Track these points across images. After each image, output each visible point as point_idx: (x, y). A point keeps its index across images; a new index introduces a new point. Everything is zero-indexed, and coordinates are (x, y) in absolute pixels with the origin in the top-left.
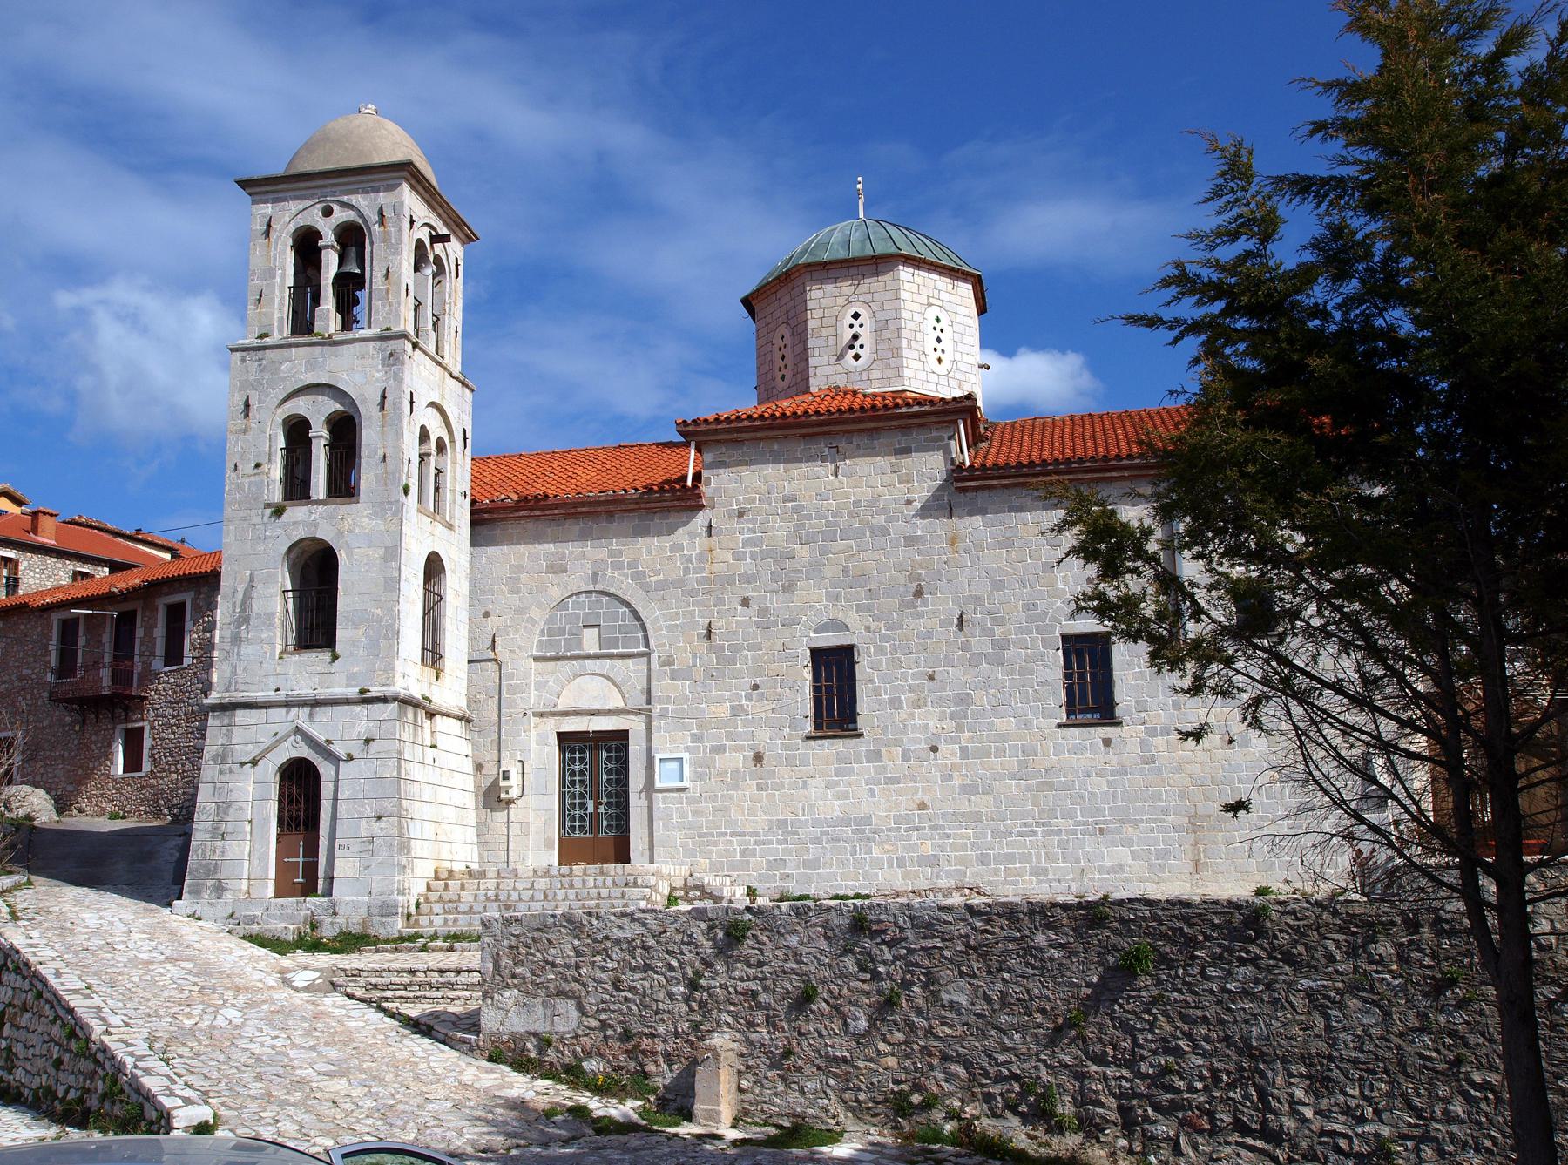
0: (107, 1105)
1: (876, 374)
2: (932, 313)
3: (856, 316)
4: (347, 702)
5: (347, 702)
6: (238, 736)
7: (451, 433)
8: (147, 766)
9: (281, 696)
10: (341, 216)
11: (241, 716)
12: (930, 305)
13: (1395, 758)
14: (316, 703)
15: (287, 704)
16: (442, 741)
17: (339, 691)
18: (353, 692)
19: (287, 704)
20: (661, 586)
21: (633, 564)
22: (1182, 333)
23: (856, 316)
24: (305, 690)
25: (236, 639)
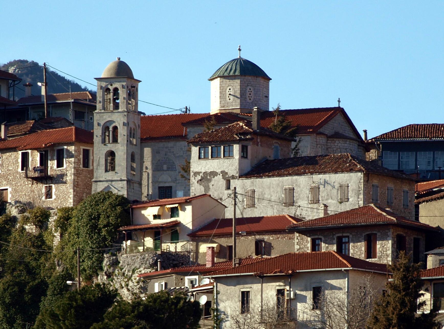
0: (52, 164)
1: (234, 104)
2: (249, 87)
3: (230, 89)
4: (118, 181)
5: (118, 181)
6: (98, 187)
7: (136, 126)
8: (54, 197)
9: (106, 180)
10: (114, 86)
11: (99, 183)
12: (248, 86)
13: (321, 130)
14: (112, 181)
15: (107, 181)
16: (135, 188)
17: (115, 178)
18: (119, 179)
19: (107, 181)
20: (179, 156)
21: (173, 152)
22: (255, 276)
23: (230, 89)
24: (110, 179)
25: (97, 169)
